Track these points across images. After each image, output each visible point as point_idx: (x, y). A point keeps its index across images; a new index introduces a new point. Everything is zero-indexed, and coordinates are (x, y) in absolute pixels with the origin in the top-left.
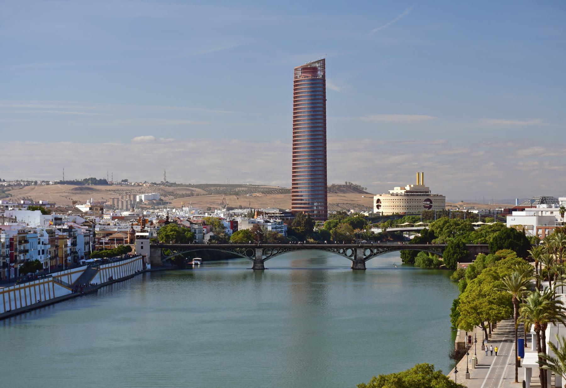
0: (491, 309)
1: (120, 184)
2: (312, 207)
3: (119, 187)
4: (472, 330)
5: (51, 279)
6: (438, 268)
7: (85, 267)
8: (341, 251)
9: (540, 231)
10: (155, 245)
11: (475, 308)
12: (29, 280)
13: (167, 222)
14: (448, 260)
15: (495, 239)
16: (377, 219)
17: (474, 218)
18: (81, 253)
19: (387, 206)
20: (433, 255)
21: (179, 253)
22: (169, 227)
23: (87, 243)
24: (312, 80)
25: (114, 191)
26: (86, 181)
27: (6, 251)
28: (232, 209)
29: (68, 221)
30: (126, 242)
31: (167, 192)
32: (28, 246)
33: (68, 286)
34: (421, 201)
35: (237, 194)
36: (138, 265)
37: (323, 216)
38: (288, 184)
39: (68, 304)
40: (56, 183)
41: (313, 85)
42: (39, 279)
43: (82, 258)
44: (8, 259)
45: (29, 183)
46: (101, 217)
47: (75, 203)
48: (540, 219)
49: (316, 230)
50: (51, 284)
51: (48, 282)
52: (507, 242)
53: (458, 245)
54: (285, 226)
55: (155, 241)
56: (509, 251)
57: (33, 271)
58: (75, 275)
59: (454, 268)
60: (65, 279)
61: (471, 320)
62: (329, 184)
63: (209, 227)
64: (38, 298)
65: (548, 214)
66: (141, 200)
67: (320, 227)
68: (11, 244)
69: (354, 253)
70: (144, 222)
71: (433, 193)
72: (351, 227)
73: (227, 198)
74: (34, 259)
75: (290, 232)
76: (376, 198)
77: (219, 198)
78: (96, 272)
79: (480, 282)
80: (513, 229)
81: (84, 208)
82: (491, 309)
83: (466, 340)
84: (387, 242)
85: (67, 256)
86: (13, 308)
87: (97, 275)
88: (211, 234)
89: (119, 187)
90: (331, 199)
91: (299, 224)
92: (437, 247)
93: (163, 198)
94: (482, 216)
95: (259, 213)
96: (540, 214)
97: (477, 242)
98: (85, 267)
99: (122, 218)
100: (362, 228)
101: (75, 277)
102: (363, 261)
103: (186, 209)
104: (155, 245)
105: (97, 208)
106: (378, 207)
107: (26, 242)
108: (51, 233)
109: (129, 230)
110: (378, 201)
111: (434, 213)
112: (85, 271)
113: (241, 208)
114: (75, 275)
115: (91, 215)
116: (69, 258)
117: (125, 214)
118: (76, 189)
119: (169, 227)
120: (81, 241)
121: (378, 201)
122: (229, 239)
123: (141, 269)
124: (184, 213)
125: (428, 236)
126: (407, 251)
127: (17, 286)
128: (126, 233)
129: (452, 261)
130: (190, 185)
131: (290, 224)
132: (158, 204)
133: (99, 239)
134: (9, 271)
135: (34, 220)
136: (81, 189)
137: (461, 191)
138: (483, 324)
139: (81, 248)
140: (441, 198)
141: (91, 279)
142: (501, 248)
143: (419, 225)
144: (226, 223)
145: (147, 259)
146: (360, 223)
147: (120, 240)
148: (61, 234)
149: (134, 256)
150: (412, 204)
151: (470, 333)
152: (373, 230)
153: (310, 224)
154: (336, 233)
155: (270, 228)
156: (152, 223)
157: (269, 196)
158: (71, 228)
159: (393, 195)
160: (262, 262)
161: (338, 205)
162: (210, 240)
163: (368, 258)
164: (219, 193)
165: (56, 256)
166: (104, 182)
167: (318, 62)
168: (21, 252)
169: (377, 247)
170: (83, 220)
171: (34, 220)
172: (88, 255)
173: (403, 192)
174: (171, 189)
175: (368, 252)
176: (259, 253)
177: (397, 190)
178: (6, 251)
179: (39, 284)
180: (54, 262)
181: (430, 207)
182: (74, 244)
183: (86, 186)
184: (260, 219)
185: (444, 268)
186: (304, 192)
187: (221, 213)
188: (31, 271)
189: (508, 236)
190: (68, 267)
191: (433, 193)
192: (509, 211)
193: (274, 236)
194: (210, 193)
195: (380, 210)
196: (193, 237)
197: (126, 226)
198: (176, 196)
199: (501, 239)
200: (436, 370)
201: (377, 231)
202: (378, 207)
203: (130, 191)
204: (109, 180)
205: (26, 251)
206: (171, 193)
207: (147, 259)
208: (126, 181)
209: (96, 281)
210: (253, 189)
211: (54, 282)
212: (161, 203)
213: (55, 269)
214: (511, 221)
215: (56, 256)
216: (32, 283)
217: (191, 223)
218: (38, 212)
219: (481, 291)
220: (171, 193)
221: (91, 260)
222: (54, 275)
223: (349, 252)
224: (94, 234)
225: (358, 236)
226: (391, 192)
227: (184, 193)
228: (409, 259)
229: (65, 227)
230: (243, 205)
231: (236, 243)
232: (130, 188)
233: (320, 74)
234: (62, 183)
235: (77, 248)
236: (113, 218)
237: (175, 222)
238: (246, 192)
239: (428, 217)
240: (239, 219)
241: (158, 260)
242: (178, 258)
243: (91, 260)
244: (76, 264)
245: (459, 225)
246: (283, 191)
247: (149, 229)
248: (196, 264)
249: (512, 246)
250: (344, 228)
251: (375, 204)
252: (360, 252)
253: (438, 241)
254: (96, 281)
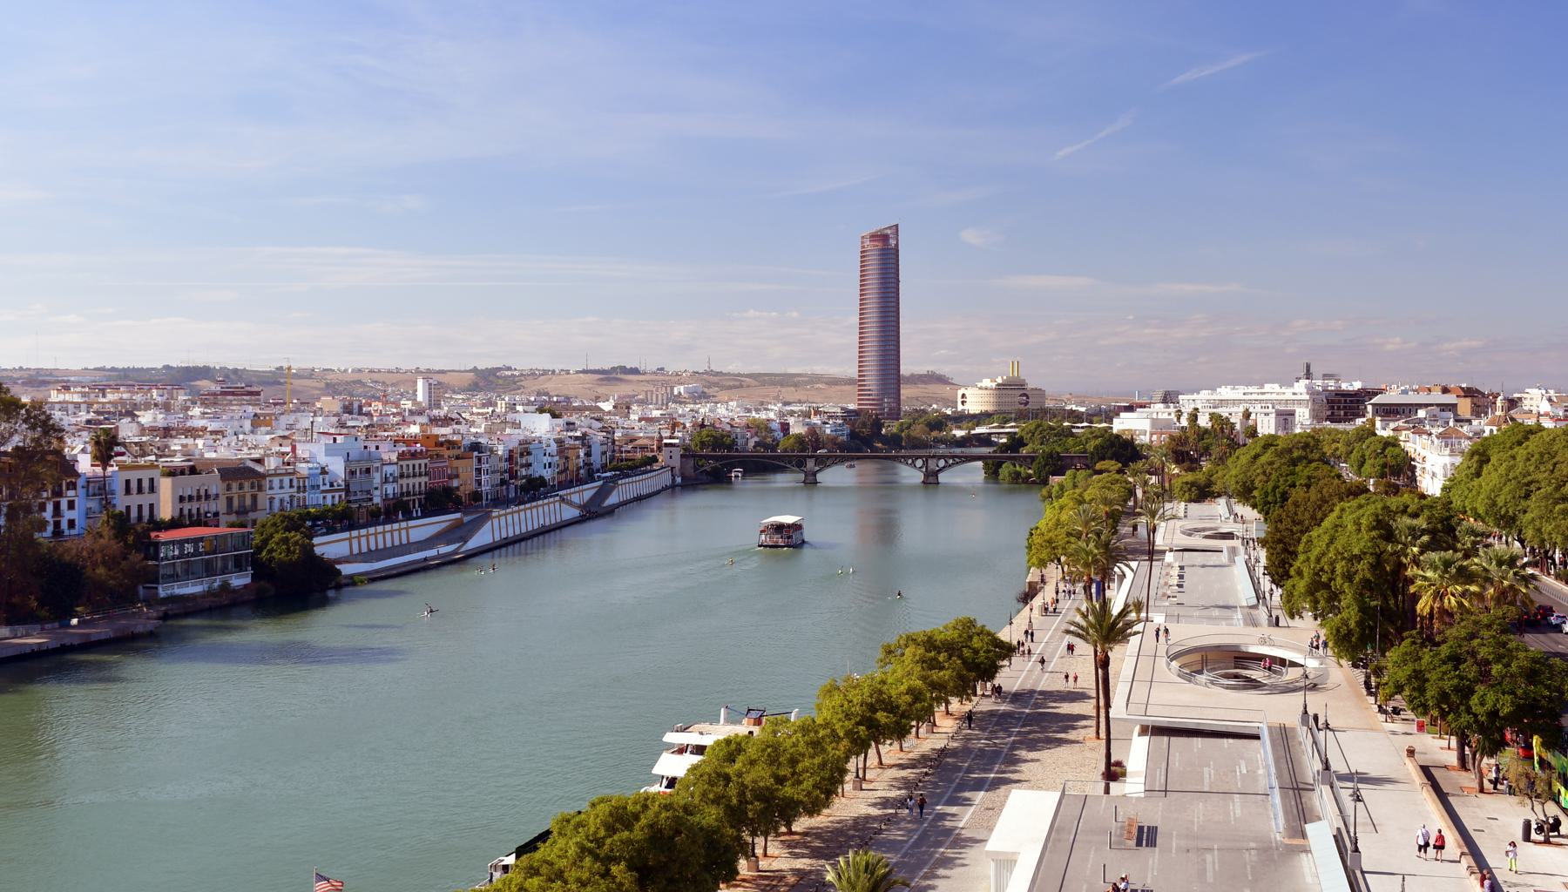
7: (600, 483)
10: (687, 453)
11: (1050, 541)
12: (530, 501)
13: (702, 426)
14: (1038, 472)
15: (1096, 447)
16: (960, 419)
17: (1076, 417)
18: (597, 465)
19: (975, 401)
21: (715, 462)
22: (705, 432)
27: (505, 465)
28: (788, 404)
29: (583, 423)
31: (711, 384)
32: (530, 459)
34: (1016, 397)
35: (795, 385)
36: (665, 479)
37: (895, 414)
38: (852, 371)
41: (885, 255)
45: (545, 372)
46: (627, 416)
48: (1155, 422)
49: (885, 435)
52: (1110, 453)
53: (1050, 455)
54: (847, 429)
58: (587, 492)
59: (1045, 482)
60: (575, 498)
61: (1044, 556)
62: (905, 369)
65: (1165, 416)
67: (890, 428)
68: (510, 458)
69: (926, 463)
70: (674, 426)
71: (1030, 386)
76: (960, 393)
78: (613, 488)
79: (1061, 508)
81: (607, 406)
83: (1037, 579)
84: (962, 451)
85: (579, 469)
86: (511, 534)
90: (906, 392)
91: (864, 424)
92: (1025, 458)
95: (817, 412)
97: (1075, 450)
98: (600, 483)
99: (650, 420)
101: (588, 495)
102: (936, 474)
104: (687, 453)
105: (623, 407)
107: (529, 454)
108: (559, 442)
112: (601, 487)
114: (587, 492)
117: (656, 413)
119: (705, 432)
120: (596, 451)
124: (727, 412)
125: (1016, 443)
130: (739, 375)
135: (541, 427)
136: (608, 379)
137: (1064, 383)
139: (597, 460)
140: (1040, 393)
142: (1103, 459)
144: (775, 426)
145: (677, 471)
146: (939, 423)
147: (643, 448)
153: (878, 425)
154: (909, 436)
155: (828, 431)
158: (585, 435)
164: (773, 384)
165: (566, 469)
166: (635, 371)
169: (953, 457)
171: (541, 427)
172: (604, 468)
174: (715, 379)
175: (942, 463)
176: (810, 464)
177: (987, 383)
178: (505, 465)
180: (563, 477)
182: (588, 454)
184: (816, 420)
186: (872, 382)
188: (534, 489)
189: (1112, 445)
190: (581, 482)
191: (1030, 386)
192: (1117, 412)
193: (833, 440)
194: (763, 384)
196: (734, 442)
197: (653, 431)
200: (979, 624)
201: (959, 433)
204: (642, 369)
206: (716, 384)
207: (677, 471)
209: (612, 500)
210: (815, 379)
212: (700, 397)
213: (565, 485)
220: (716, 384)
223: (919, 463)
224: (614, 441)
225: (938, 441)
229: (578, 434)
230: (803, 398)
233: (893, 242)
234: (584, 372)
237: (712, 425)
238: (807, 383)
239: (1021, 416)
240: (791, 420)
241: (690, 472)
242: (715, 470)
244: (590, 478)
246: (850, 382)
249: (1116, 457)
250: (918, 431)
252: (932, 464)
254: (612, 500)
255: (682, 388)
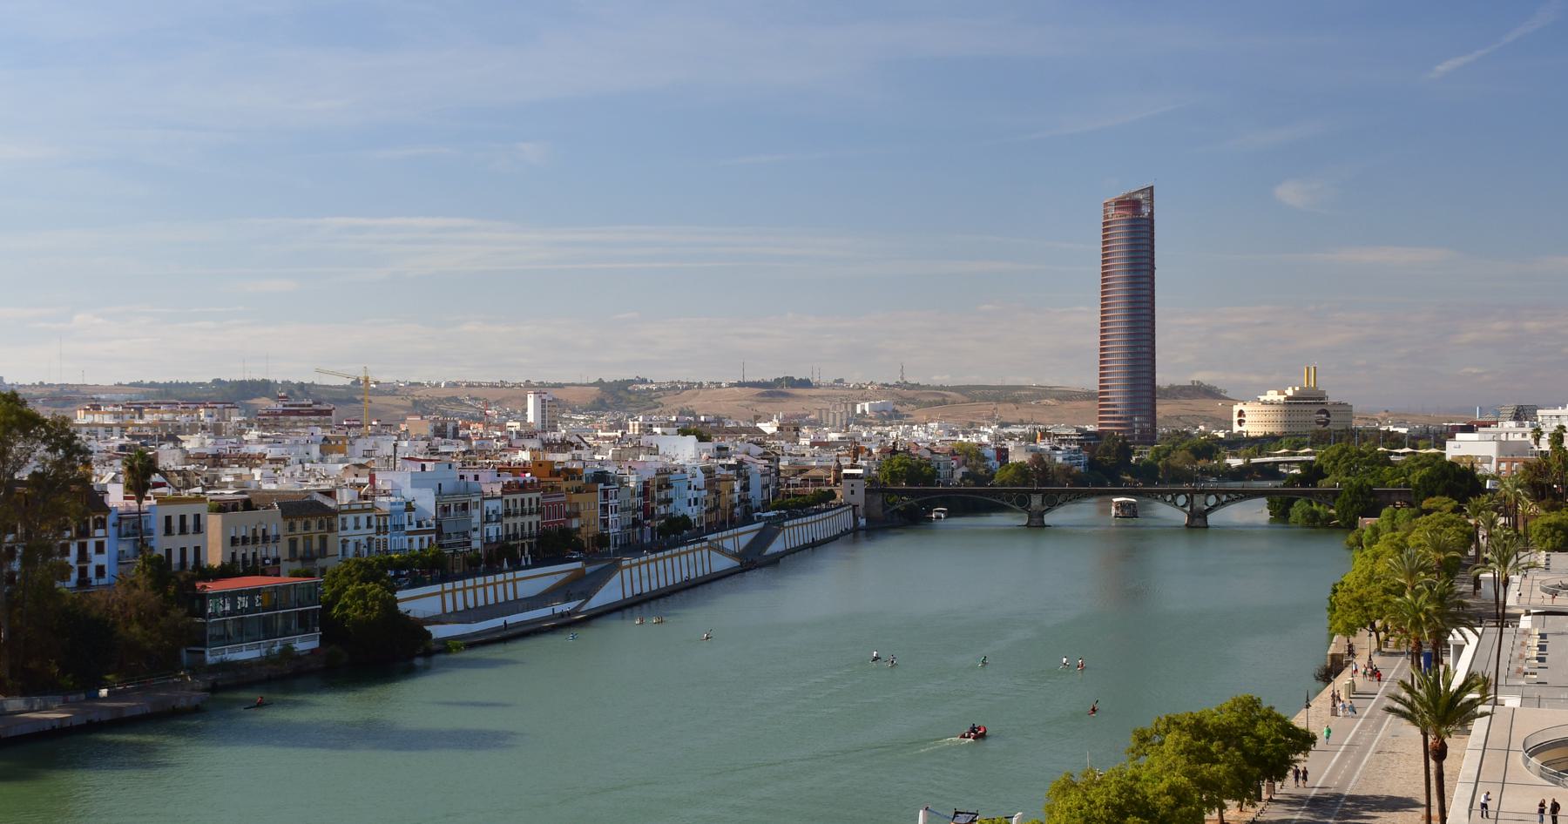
0: (1386, 601)
1: (831, 386)
2: (1130, 425)
3: (830, 391)
4: (1354, 634)
5: (705, 544)
6: (1327, 526)
7: (760, 525)
8: (1169, 498)
9: (1503, 466)
10: (874, 487)
11: (1360, 600)
12: (671, 547)
13: (894, 451)
15: (1422, 479)
16: (1237, 443)
19: (1254, 421)
20: (1319, 504)
21: (910, 497)
22: (896, 460)
23: (766, 487)
24: (1132, 220)
25: (822, 397)
26: (778, 380)
28: (1007, 425)
29: (738, 449)
30: (828, 484)
31: (906, 399)
32: (671, 493)
33: (734, 555)
34: (1312, 415)
35: (1016, 401)
36: (844, 520)
37: (1149, 437)
38: (1092, 382)
39: (735, 578)
40: (731, 385)
41: (1135, 228)
42: (687, 544)
43: (758, 510)
44: (640, 514)
45: (689, 386)
46: (796, 440)
47: (757, 418)
48: (1503, 446)
49: (1138, 463)
50: (705, 552)
51: (701, 549)
53: (1360, 490)
54: (1084, 457)
55: (873, 481)
56: (1446, 499)
57: (678, 532)
58: (743, 537)
59: (1352, 526)
60: (729, 544)
61: (1352, 619)
63: (961, 458)
64: (685, 575)
65: (1518, 437)
66: (864, 411)
67: (1143, 455)
69: (1190, 501)
70: (857, 452)
72: (1192, 457)
73: (1000, 407)
74: (679, 514)
75: (1092, 464)
76: (1236, 409)
77: (986, 408)
78: (777, 533)
79: (1376, 556)
80: (1452, 464)
81: (769, 428)
82: (1386, 601)
83: (1343, 650)
84: (1239, 486)
85: (733, 506)
86: (646, 589)
87: (780, 538)
88: (964, 469)
89: (830, 391)
90: (1163, 409)
91: (1107, 451)
93: (898, 408)
94: (1412, 438)
95: (1045, 434)
96: (1503, 437)
98: (760, 525)
100: (1210, 458)
101: (744, 540)
102: (1204, 515)
103: (934, 425)
105: (790, 429)
106: (1240, 422)
107: (669, 486)
108: (708, 471)
109: (833, 464)
110: (1241, 413)
111: (1329, 433)
112: (761, 530)
113: (1022, 423)
114: (743, 537)
115: (779, 439)
116: (737, 510)
117: (834, 436)
118: (762, 395)
119: (896, 460)
120: (756, 483)
121: (1241, 413)
122: (993, 477)
123: (850, 526)
124: (925, 434)
125: (1313, 473)
126: (1277, 498)
127: (652, 557)
128: (828, 468)
129: (1350, 515)
130: (942, 388)
131: (1092, 452)
132: (890, 417)
133: (787, 479)
134: (642, 532)
135: (685, 452)
136: (770, 394)
137: (1379, 397)
138: (1373, 625)
139: (756, 494)
140: (1345, 408)
141: (765, 548)
143: (1306, 454)
144: (990, 452)
145: (860, 511)
146: (1209, 448)
147: (817, 481)
148: (724, 472)
149: (841, 505)
150: (1295, 418)
151: (1352, 639)
152: (1228, 461)
153: (1125, 451)
154: (1167, 466)
155: (1059, 460)
156: (870, 453)
157: (1067, 405)
158: (741, 463)
159: (1264, 403)
160: (1041, 515)
161: (1178, 418)
162: (962, 479)
163: (1211, 509)
164: (986, 399)
165: (717, 507)
166: (806, 384)
167: (1142, 191)
168: (660, 502)
170: (761, 450)
171: (685, 452)
172: (766, 506)
173: (1282, 398)
174: (911, 393)
175: (1212, 500)
176: (1036, 501)
177: (1272, 395)
179: (687, 553)
181: (1327, 423)
182: (745, 488)
183: (778, 389)
184: (1043, 445)
185: (1337, 526)
186: (1118, 396)
187: (985, 436)
188: (675, 532)
189: (1445, 475)
193: (1066, 471)
195: (1243, 428)
196: (935, 473)
197: (829, 458)
198: (919, 404)
199: (1432, 479)
201: (1235, 462)
202: (1240, 422)
203: (847, 397)
205: (669, 501)
206: (911, 400)
207: (860, 511)
208: (841, 381)
210: (1042, 393)
211: (710, 548)
212: (890, 416)
213: (712, 528)
214: (1461, 447)
215: (717, 507)
216: (676, 551)
217: (932, 452)
218: (692, 439)
219: (1372, 572)
220: (911, 400)
221: (771, 514)
222: (710, 537)
223: (1181, 500)
224: (778, 472)
225: (1206, 472)
226: (1262, 398)
227: (932, 399)
228: (1281, 511)
229: (733, 462)
230: (1026, 418)
231: (1003, 484)
232: (847, 392)
233: (1145, 210)
234: (740, 385)
235: (751, 494)
236: (813, 445)
237: (907, 451)
238: (1031, 398)
239: (1319, 439)
240: (1011, 446)
241: (878, 511)
243: (771, 514)
244: (747, 519)
245: (1364, 455)
246: (1089, 396)
247: (864, 463)
248: (939, 518)
249: (1450, 492)
250: (1179, 459)
251: (1236, 418)
252: (1198, 501)
253: (1323, 484)
254: (777, 546)
255: (867, 405)
